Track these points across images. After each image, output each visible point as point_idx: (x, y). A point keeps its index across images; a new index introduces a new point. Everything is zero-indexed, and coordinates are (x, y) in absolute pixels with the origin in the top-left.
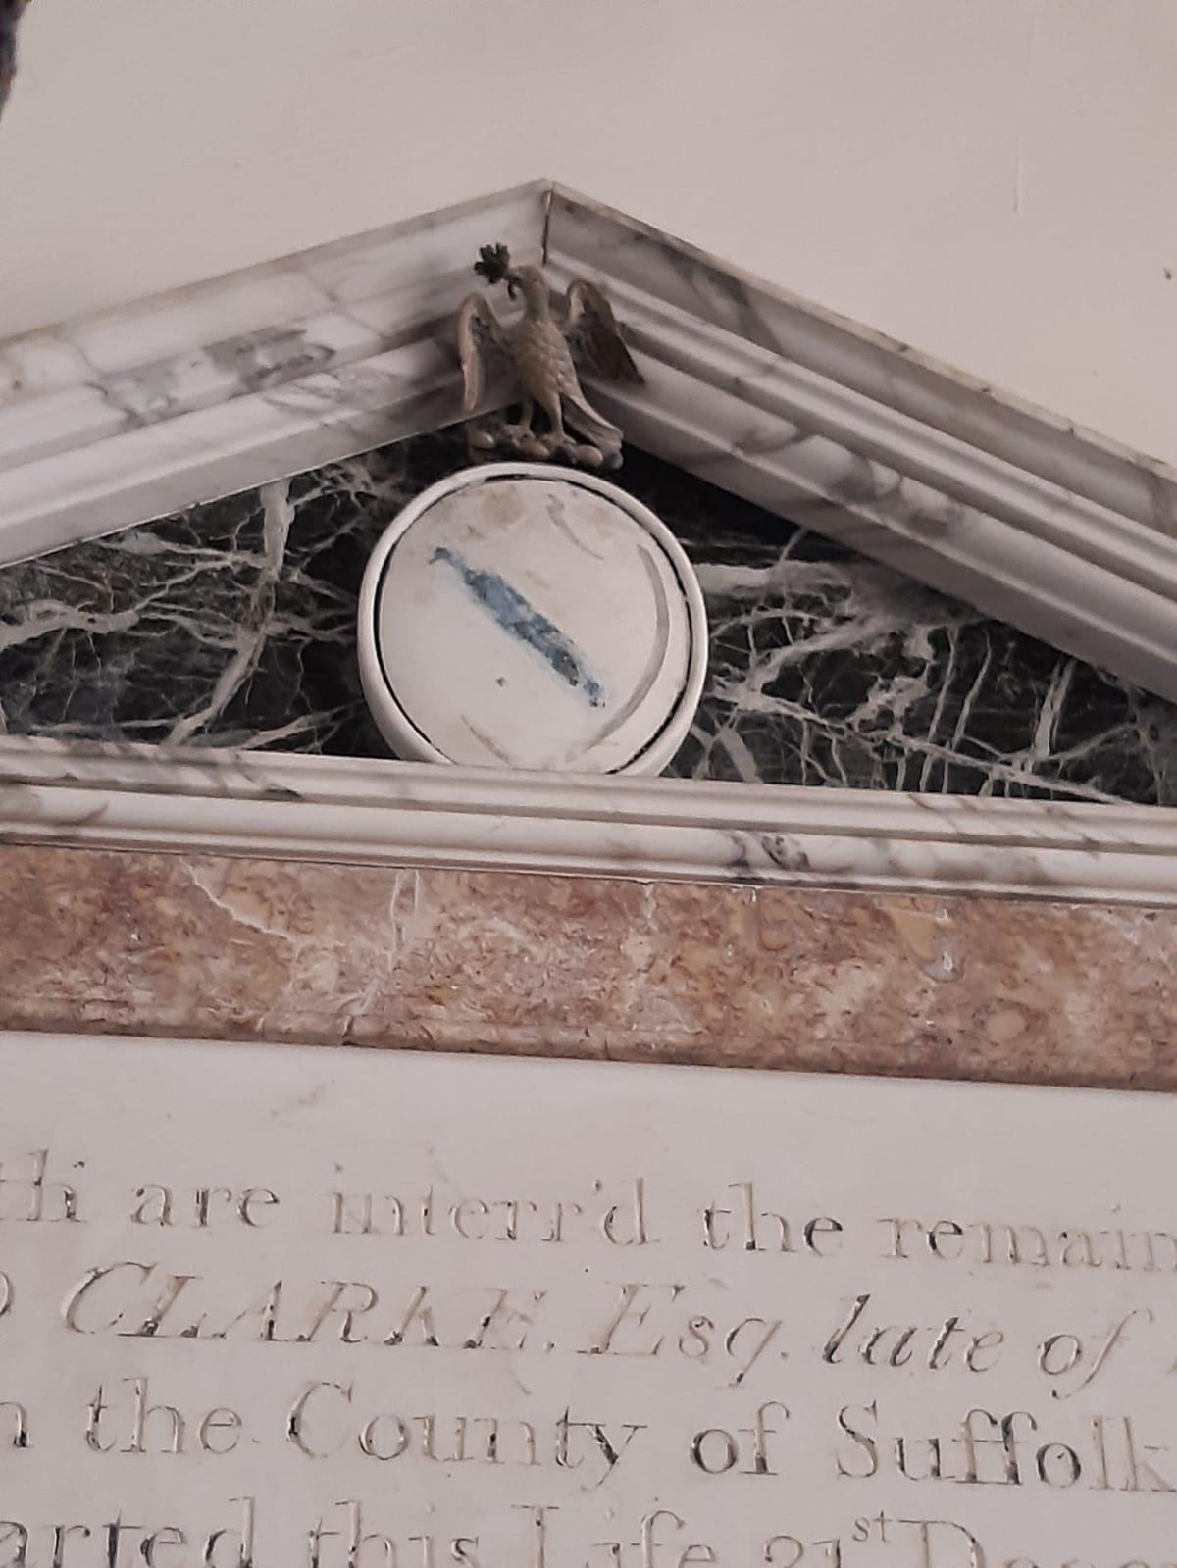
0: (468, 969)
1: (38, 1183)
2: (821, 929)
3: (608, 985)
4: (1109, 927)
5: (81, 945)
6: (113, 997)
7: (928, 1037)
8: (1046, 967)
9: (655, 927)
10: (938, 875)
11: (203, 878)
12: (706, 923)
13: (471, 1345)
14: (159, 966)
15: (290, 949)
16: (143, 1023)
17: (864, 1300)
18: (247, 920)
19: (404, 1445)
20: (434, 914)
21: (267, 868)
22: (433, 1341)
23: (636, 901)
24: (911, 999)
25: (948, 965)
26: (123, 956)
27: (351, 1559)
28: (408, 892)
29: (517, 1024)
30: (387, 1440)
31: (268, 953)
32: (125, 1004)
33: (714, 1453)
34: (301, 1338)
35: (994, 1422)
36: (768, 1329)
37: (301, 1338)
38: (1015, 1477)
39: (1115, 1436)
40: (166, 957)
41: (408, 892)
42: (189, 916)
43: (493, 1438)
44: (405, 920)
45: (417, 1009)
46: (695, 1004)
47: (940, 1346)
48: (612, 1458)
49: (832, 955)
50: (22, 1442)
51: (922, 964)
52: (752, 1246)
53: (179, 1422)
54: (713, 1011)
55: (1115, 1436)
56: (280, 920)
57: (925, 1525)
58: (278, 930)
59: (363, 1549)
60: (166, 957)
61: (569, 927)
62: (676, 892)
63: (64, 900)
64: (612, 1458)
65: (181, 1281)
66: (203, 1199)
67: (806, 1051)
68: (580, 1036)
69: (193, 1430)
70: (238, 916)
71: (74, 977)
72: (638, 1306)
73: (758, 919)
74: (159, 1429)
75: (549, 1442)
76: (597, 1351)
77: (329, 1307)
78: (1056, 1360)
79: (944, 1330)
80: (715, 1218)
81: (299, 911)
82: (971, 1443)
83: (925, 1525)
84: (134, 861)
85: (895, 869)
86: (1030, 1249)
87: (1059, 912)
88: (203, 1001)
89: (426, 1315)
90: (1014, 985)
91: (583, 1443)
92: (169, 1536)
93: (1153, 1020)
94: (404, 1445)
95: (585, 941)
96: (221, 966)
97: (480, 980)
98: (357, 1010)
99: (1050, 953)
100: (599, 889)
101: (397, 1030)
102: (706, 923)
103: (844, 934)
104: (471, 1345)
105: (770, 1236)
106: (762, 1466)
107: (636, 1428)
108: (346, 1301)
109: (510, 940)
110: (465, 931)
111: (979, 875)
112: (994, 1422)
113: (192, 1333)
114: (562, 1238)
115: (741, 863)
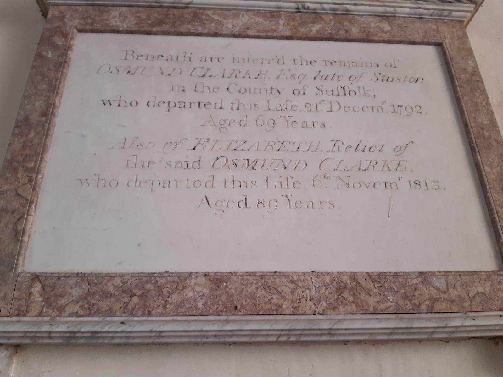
0: (253, 25)
1: (185, 56)
2: (312, 19)
3: (277, 27)
4: (359, 19)
5: (190, 22)
6: (195, 29)
7: (330, 34)
8: (348, 24)
9: (284, 19)
10: (330, 10)
11: (210, 13)
12: (292, 18)
13: (256, 78)
14: (203, 25)
15: (224, 22)
16: (200, 33)
17: (320, 71)
18: (216, 18)
19: (246, 92)
20: (247, 18)
21: (220, 12)
22: (250, 78)
23: (281, 16)
24: (326, 28)
25: (332, 24)
26: (197, 23)
27: (238, 107)
28: (243, 14)
29: (262, 32)
30: (243, 91)
31: (221, 23)
32: (197, 30)
33: (296, 92)
34: (228, 77)
35: (342, 87)
36: (304, 76)
37: (228, 77)
38: (345, 95)
39: (361, 89)
40: (203, 23)
41: (243, 14)
42: (207, 18)
43: (260, 91)
44: (243, 19)
45: (245, 30)
46: (291, 30)
47: (333, 77)
48: (279, 93)
49: (314, 23)
50: (184, 91)
51: (328, 24)
52: (301, 64)
53: (209, 88)
54: (294, 30)
55: (361, 89)
56: (222, 18)
57: (331, 102)
58: (222, 20)
59: (240, 105)
60: (203, 23)
61: (270, 19)
62: (287, 14)
63: (187, 16)
64: (279, 93)
65: (208, 69)
66: (211, 58)
67: (310, 36)
68: (272, 34)
69: (211, 90)
70: (215, 18)
71: (189, 26)
72: (283, 73)
73: (301, 18)
74: (206, 90)
75: (269, 91)
76: (276, 79)
77: (233, 73)
78: (351, 79)
79: (333, 75)
80: (296, 61)
81: (226, 17)
82: (338, 90)
83: (331, 102)
84: (198, 10)
85: (323, 9)
86: (347, 64)
87: (351, 17)
88: (210, 29)
89: (249, 74)
90: (343, 27)
91: (275, 91)
92: (208, 104)
93: (366, 31)
94: (246, 92)
95: (273, 21)
96: (213, 25)
97: (255, 26)
98: (235, 31)
99: (349, 22)
100: (275, 14)
101: (242, 33)
102: (292, 18)
103: (315, 20)
104: (256, 78)
105: (304, 63)
106: (304, 94)
107: (283, 89)
108: (236, 72)
109: (260, 21)
110: (253, 20)
111: (337, 10)
112: (342, 87)
113: (211, 76)
114: (285, 63)
115: (298, 8)
